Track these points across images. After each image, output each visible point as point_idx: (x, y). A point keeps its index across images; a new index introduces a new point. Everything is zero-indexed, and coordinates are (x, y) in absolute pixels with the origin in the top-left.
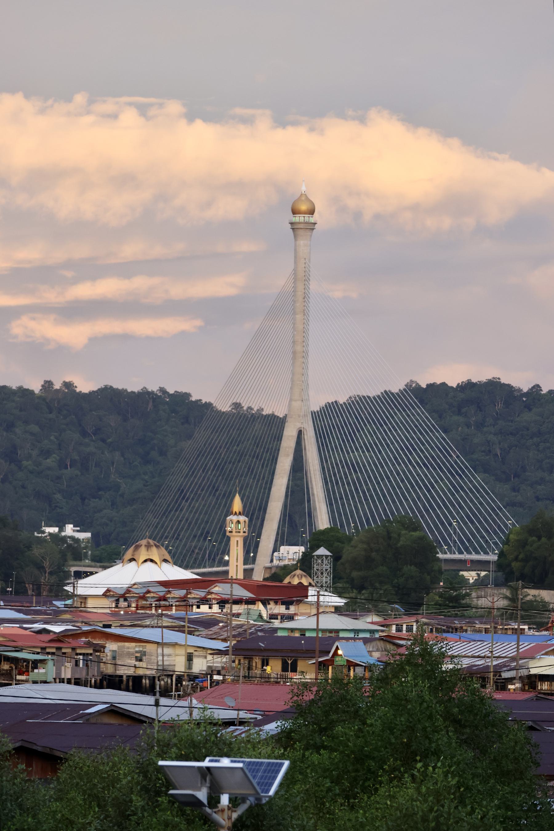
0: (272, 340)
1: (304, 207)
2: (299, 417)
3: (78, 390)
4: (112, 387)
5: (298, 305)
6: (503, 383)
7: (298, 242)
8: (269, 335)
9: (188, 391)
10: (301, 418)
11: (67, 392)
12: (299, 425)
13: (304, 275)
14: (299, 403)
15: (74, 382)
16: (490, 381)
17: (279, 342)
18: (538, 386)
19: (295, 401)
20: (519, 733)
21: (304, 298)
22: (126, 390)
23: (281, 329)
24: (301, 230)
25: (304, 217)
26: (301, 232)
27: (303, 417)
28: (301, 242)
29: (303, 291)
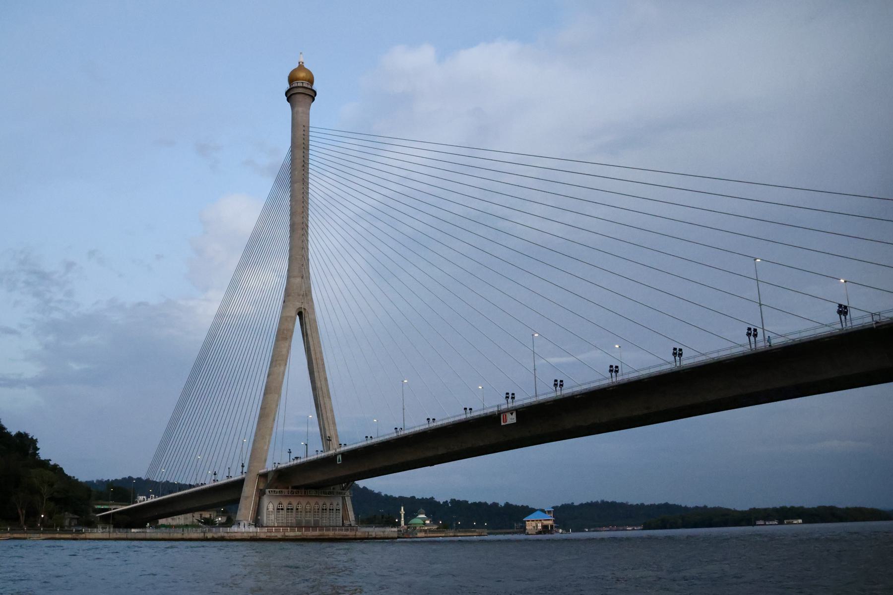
0: (208, 363)
1: (302, 75)
2: (299, 295)
3: (470, 502)
4: (557, 507)
5: (296, 173)
6: (606, 501)
7: (296, 109)
8: (221, 339)
9: (431, 497)
10: (301, 297)
11: (403, 506)
12: (298, 305)
13: (302, 187)
14: (298, 280)
15: (707, 505)
16: (474, 503)
17: (240, 308)
18: (433, 497)
19: (294, 277)
20: (326, 574)
21: (303, 166)
22: (466, 502)
23: (229, 328)
24: (298, 96)
25: (303, 83)
26: (299, 98)
27: (303, 295)
28: (300, 109)
29: (303, 159)
